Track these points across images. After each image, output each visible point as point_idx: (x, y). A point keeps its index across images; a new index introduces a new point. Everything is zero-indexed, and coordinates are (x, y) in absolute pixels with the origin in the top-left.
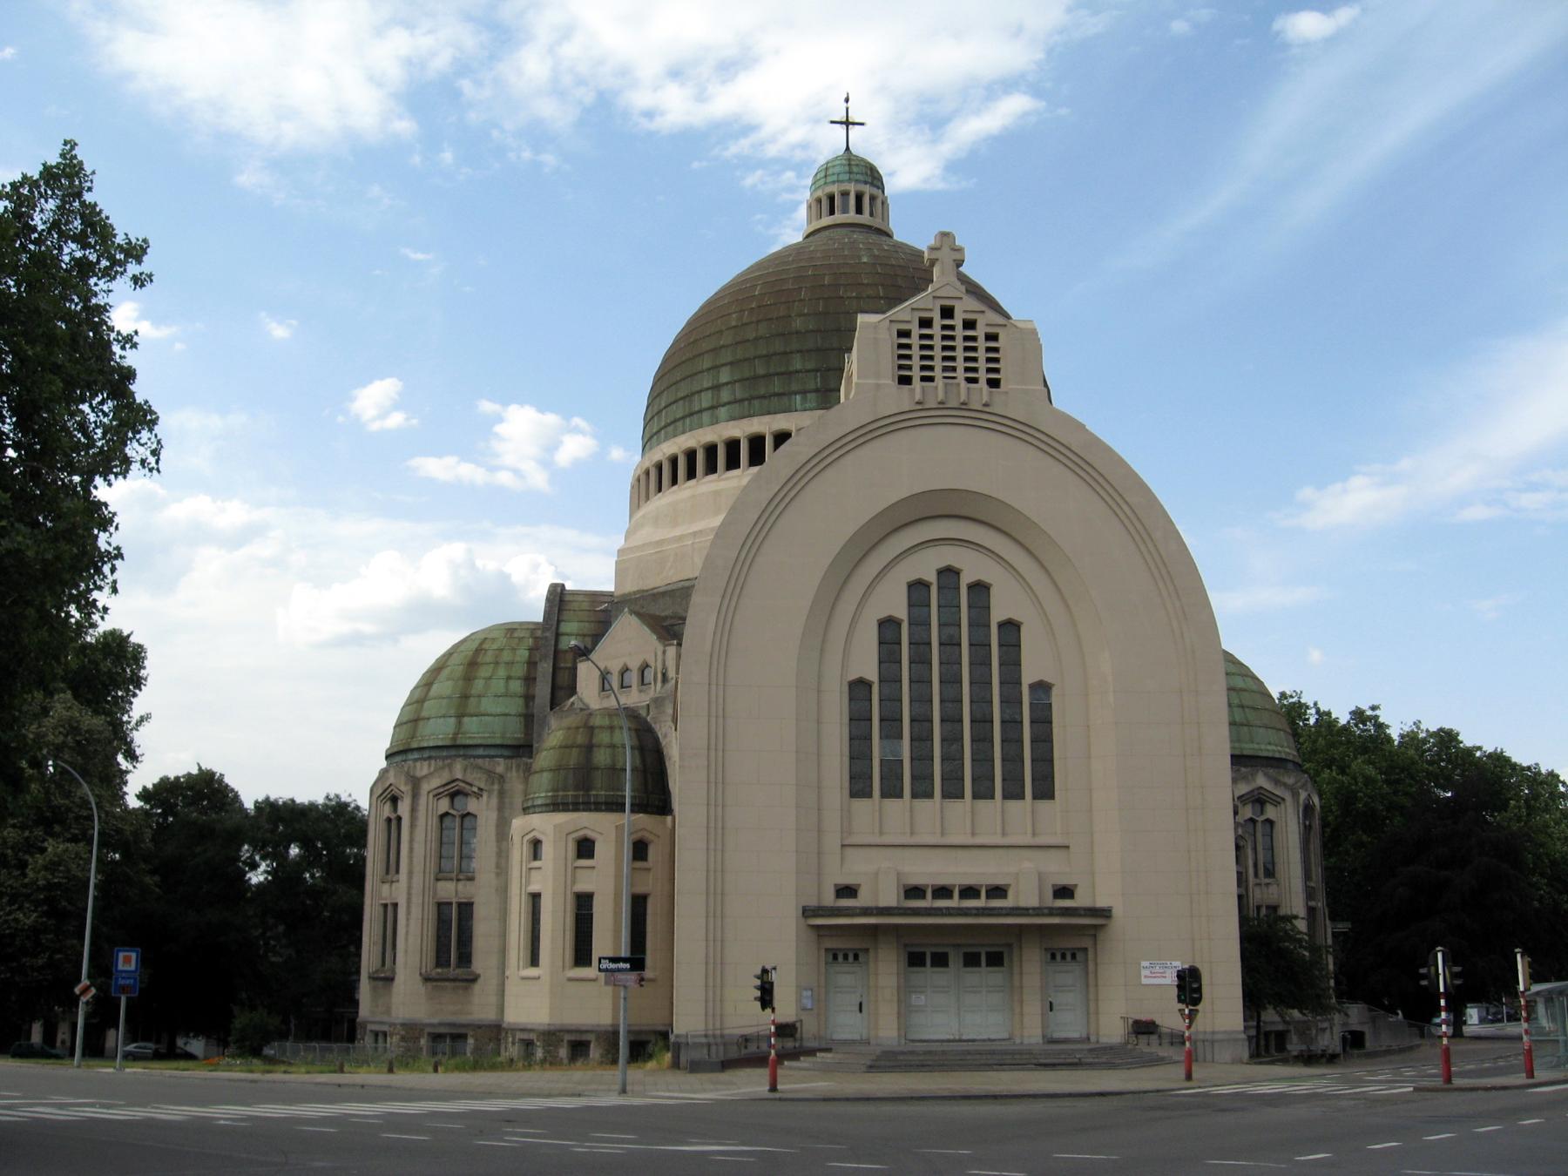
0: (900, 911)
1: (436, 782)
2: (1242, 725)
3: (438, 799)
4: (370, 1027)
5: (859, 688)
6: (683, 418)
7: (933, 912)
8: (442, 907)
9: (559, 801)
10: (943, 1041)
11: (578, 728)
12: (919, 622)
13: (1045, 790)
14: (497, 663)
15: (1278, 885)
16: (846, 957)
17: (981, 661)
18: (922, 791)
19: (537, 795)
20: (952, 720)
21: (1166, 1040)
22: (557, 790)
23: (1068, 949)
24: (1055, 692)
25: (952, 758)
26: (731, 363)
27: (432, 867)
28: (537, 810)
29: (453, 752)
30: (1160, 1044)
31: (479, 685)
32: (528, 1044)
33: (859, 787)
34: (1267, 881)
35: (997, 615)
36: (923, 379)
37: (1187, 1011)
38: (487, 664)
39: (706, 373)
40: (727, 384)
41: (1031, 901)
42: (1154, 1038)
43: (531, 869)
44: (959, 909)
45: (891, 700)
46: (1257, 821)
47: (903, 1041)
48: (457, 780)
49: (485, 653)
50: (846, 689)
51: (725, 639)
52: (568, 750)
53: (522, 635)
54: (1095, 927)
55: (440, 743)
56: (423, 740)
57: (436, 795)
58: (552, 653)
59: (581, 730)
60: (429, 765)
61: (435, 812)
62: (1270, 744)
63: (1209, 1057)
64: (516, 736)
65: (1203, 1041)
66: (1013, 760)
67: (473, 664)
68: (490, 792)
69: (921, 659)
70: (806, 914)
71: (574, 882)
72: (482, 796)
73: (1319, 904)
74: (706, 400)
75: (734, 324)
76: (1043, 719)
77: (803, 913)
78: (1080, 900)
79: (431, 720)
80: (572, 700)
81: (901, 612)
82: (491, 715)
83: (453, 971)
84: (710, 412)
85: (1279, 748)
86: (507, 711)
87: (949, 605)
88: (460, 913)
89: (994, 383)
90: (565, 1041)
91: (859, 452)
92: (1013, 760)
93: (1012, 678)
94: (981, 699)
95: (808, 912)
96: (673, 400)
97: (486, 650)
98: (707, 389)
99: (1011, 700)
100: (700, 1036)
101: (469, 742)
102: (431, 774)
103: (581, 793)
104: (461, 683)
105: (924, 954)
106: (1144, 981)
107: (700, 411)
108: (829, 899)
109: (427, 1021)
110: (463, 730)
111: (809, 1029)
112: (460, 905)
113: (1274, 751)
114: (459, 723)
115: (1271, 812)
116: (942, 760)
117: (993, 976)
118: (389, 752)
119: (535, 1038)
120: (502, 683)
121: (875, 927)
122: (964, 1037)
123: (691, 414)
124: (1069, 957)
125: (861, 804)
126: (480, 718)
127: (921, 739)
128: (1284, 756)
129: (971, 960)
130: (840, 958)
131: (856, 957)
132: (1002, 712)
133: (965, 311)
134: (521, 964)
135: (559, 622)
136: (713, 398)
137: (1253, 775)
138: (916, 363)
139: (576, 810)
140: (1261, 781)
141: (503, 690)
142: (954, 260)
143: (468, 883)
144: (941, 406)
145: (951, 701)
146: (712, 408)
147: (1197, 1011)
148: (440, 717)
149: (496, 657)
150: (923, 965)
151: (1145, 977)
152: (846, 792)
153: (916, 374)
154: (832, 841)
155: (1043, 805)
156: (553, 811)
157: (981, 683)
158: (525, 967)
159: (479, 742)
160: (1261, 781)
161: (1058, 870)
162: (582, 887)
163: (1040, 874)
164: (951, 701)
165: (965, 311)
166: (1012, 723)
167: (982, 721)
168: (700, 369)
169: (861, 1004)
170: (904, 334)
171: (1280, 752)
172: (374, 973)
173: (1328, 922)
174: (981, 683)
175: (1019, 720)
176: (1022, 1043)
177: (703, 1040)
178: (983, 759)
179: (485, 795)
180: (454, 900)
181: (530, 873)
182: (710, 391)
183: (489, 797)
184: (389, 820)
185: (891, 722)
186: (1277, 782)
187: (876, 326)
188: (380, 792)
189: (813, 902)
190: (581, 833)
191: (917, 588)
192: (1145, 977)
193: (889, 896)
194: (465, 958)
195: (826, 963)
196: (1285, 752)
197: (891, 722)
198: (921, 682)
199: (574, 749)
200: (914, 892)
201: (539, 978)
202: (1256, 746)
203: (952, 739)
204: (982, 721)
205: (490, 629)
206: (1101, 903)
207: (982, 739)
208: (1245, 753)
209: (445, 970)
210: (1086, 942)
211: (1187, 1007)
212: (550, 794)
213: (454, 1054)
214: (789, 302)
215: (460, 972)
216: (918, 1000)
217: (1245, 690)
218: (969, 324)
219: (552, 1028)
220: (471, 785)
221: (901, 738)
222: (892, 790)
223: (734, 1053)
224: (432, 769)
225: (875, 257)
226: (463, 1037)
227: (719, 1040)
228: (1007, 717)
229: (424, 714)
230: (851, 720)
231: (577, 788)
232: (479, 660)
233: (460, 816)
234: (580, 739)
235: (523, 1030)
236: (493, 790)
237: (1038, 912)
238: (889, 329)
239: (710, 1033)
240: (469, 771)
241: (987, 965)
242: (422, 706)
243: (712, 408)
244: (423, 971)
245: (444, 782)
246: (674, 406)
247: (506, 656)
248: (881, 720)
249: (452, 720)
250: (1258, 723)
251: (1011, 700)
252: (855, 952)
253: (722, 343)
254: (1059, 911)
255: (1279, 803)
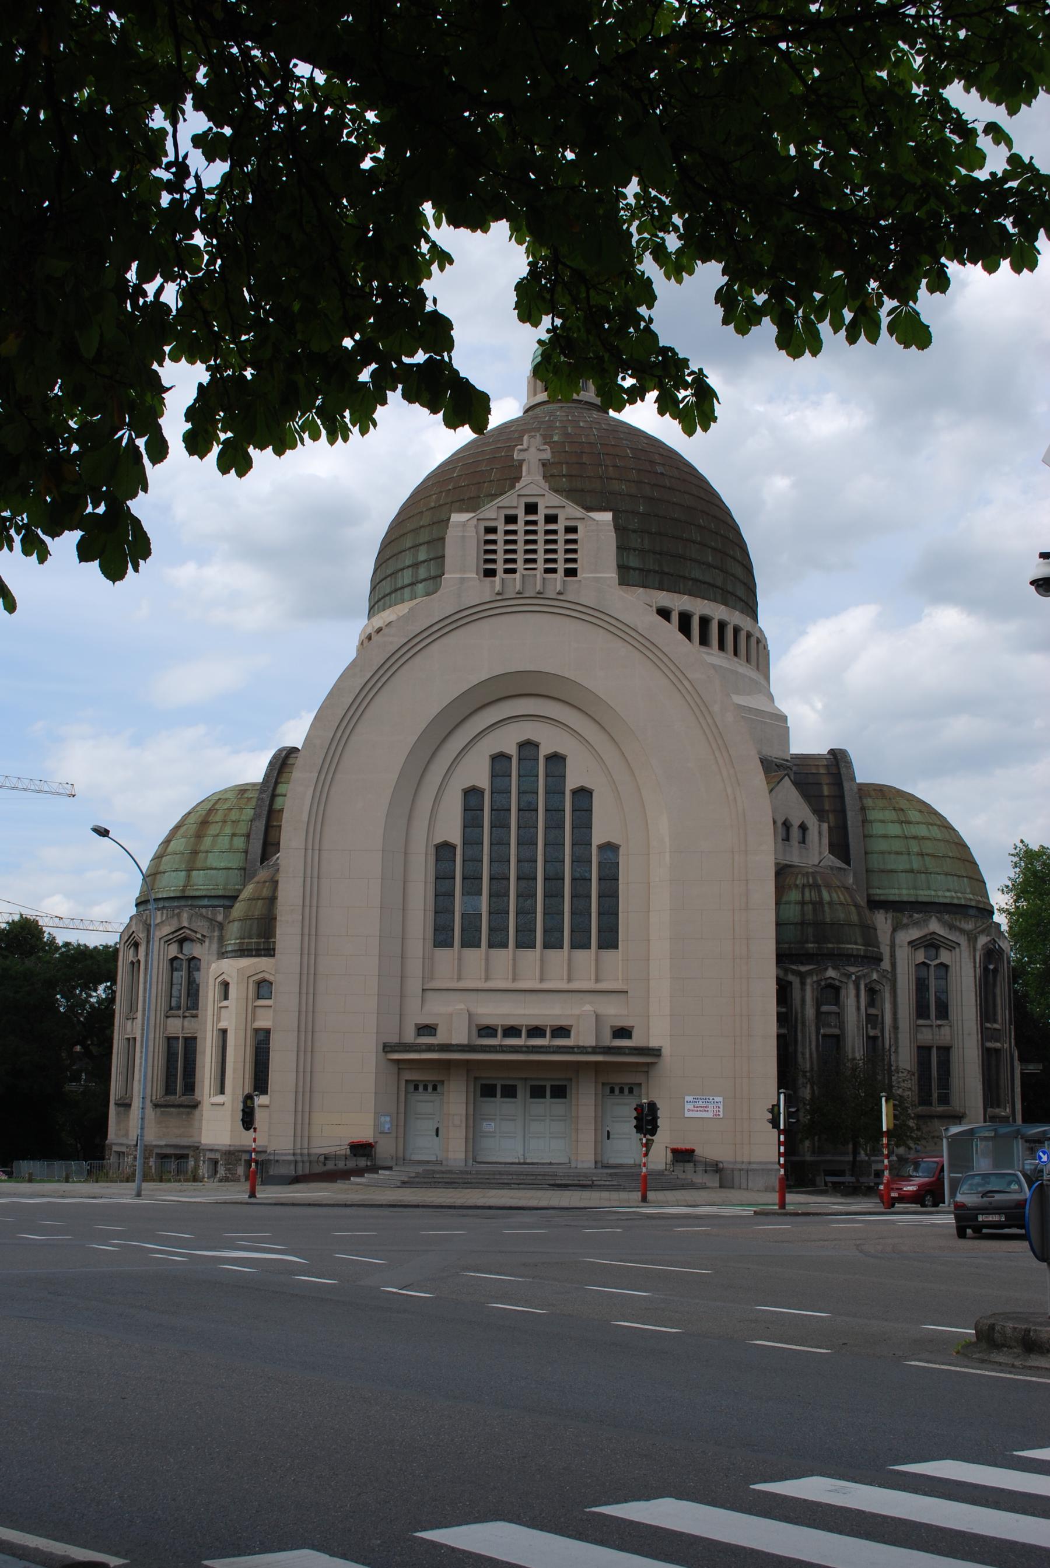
0: (460, 1048)
1: (166, 930)
2: (919, 872)
3: (168, 945)
4: (115, 1148)
5: (444, 850)
6: (390, 594)
7: (488, 1049)
8: (171, 1040)
9: (245, 947)
10: (506, 1164)
11: (265, 882)
12: (500, 790)
13: (609, 940)
14: (225, 822)
15: (951, 1026)
16: (425, 1088)
17: (555, 824)
18: (498, 942)
19: (229, 942)
20: (527, 878)
21: (700, 1169)
22: (244, 939)
23: (617, 1084)
24: (621, 851)
25: (526, 913)
26: (428, 543)
27: (163, 1005)
28: (229, 955)
29: (182, 903)
30: (695, 1172)
31: (207, 841)
32: (215, 1163)
33: (442, 937)
34: (939, 1022)
35: (572, 782)
36: (507, 571)
37: (644, 1141)
38: (217, 822)
39: (407, 552)
40: (424, 562)
41: (590, 1041)
42: (689, 1167)
43: (221, 1007)
44: (501, 1046)
45: (472, 860)
46: (930, 965)
47: (470, 1162)
48: (184, 927)
49: (216, 813)
50: (432, 851)
51: (322, 808)
52: (254, 902)
53: (251, 796)
54: (648, 1064)
55: (172, 895)
56: (158, 892)
57: (167, 941)
58: (265, 813)
59: (268, 883)
60: (162, 914)
61: (165, 956)
62: (948, 890)
63: (744, 1186)
64: (237, 887)
65: (740, 1170)
66: (581, 913)
67: (204, 823)
68: (211, 938)
69: (500, 823)
70: (386, 1050)
71: (254, 1020)
72: (204, 942)
73: (1006, 1046)
74: (407, 577)
75: (433, 505)
76: (610, 877)
77: (384, 1049)
78: (636, 1041)
79: (166, 874)
80: (278, 855)
81: (483, 781)
82: (215, 869)
83: (178, 1099)
84: (409, 588)
85: (959, 895)
86: (229, 865)
87: (528, 774)
88: (186, 1048)
89: (571, 573)
90: (243, 1160)
91: (444, 640)
92: (581, 913)
93: (582, 837)
94: (554, 860)
95: (387, 1048)
96: (383, 576)
97: (218, 810)
98: (408, 567)
99: (581, 860)
100: (289, 1154)
101: (198, 894)
102: (162, 922)
103: (263, 940)
104: (192, 839)
105: (495, 1085)
106: (687, 1114)
107: (402, 588)
108: (410, 1036)
109: (154, 1143)
110: (191, 883)
111: (385, 1149)
112: (186, 1039)
113: (952, 897)
114: (189, 876)
115: (945, 957)
116: (517, 914)
117: (557, 1107)
118: (139, 901)
119: (219, 1157)
120: (227, 839)
121: (449, 1062)
122: (528, 1161)
123: (396, 590)
124: (626, 1091)
125: (443, 953)
126: (206, 872)
127: (498, 895)
128: (963, 902)
129: (537, 1092)
130: (421, 1088)
131: (435, 1088)
132: (573, 870)
133: (547, 507)
134: (212, 1093)
135: (276, 783)
136: (412, 576)
137: (926, 922)
138: (500, 557)
139: (258, 955)
140: (935, 926)
141: (227, 846)
142: (540, 460)
143: (193, 1019)
144: (518, 596)
145: (527, 860)
146: (412, 584)
147: (653, 1140)
148: (174, 871)
149: (225, 816)
150: (544, 1097)
151: (689, 1110)
152: (430, 942)
153: (500, 567)
154: (414, 986)
155: (607, 955)
156: (241, 956)
157: (554, 845)
158: (215, 1095)
159: (204, 893)
160: (935, 926)
161: (615, 1012)
162: (262, 1023)
163: (597, 1017)
164: (527, 860)
165: (547, 507)
166: (581, 881)
167: (554, 879)
168: (404, 548)
169: (437, 1129)
170: (492, 530)
171: (958, 898)
172: (119, 1100)
173: (1017, 1063)
174: (554, 845)
175: (589, 877)
176: (576, 1168)
177: (291, 1158)
178: (553, 913)
179: (207, 941)
180: (181, 1035)
181: (255, 1009)
182: (410, 569)
183: (210, 943)
184: (132, 963)
185: (472, 880)
186: (952, 927)
187: (464, 525)
188: (126, 938)
189: (394, 1039)
190: (260, 976)
191: (499, 759)
192: (689, 1110)
193: (460, 1035)
194: (190, 1087)
195: (603, 1096)
196: (965, 898)
197: (472, 880)
198: (500, 843)
199: (260, 901)
200: (487, 1031)
201: (224, 1104)
202: (933, 893)
203: (526, 895)
204: (554, 879)
205: (226, 791)
206: (653, 1043)
207: (553, 894)
208: (920, 899)
209: (173, 1097)
210: (639, 1078)
211: (645, 1137)
212: (238, 941)
213: (179, 1172)
214: (480, 483)
215: (940, 1109)
216: (488, 1126)
217: (928, 839)
218: (551, 519)
219: (232, 1148)
220: (196, 932)
221: (481, 895)
222: (470, 941)
223: (319, 1169)
224: (164, 918)
225: (568, 435)
226: (185, 1157)
227: (306, 1158)
228: (578, 875)
229: (162, 869)
230: (437, 878)
231: (259, 936)
232: (210, 819)
233: (186, 960)
234: (266, 892)
235: (211, 1150)
236: (214, 936)
237: (595, 1050)
238: (476, 527)
239: (299, 1151)
240: (194, 919)
241: (552, 1097)
242: (161, 861)
243: (412, 584)
244: (154, 1098)
245: (173, 930)
246: (384, 582)
247: (234, 816)
248: (464, 878)
249: (183, 873)
250: (938, 870)
251: (581, 860)
252: (620, 1086)
253: (421, 524)
254: (602, 1050)
255: (954, 948)
